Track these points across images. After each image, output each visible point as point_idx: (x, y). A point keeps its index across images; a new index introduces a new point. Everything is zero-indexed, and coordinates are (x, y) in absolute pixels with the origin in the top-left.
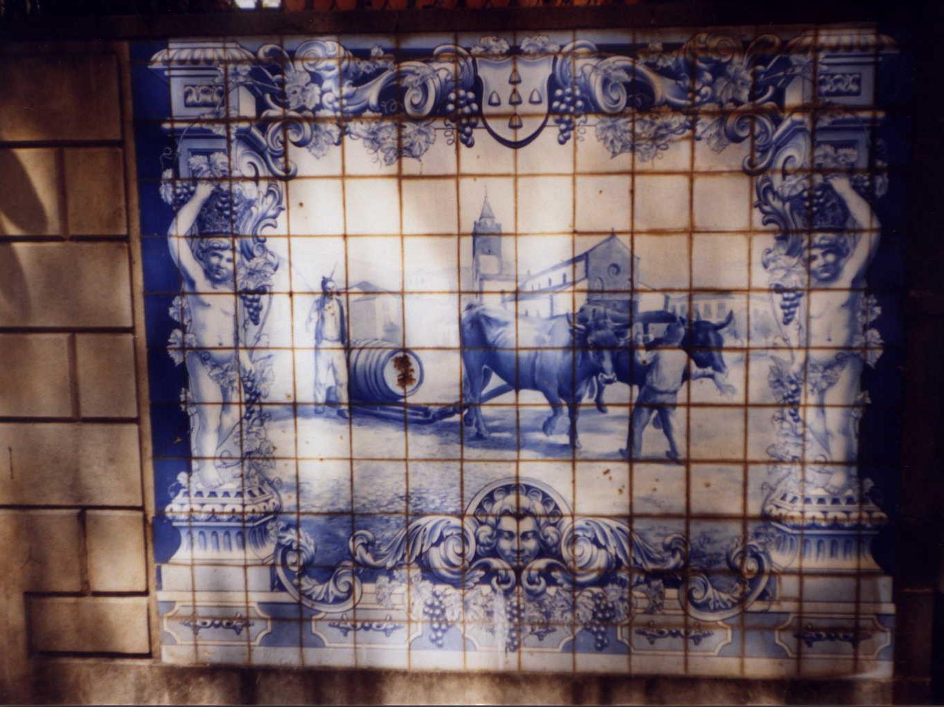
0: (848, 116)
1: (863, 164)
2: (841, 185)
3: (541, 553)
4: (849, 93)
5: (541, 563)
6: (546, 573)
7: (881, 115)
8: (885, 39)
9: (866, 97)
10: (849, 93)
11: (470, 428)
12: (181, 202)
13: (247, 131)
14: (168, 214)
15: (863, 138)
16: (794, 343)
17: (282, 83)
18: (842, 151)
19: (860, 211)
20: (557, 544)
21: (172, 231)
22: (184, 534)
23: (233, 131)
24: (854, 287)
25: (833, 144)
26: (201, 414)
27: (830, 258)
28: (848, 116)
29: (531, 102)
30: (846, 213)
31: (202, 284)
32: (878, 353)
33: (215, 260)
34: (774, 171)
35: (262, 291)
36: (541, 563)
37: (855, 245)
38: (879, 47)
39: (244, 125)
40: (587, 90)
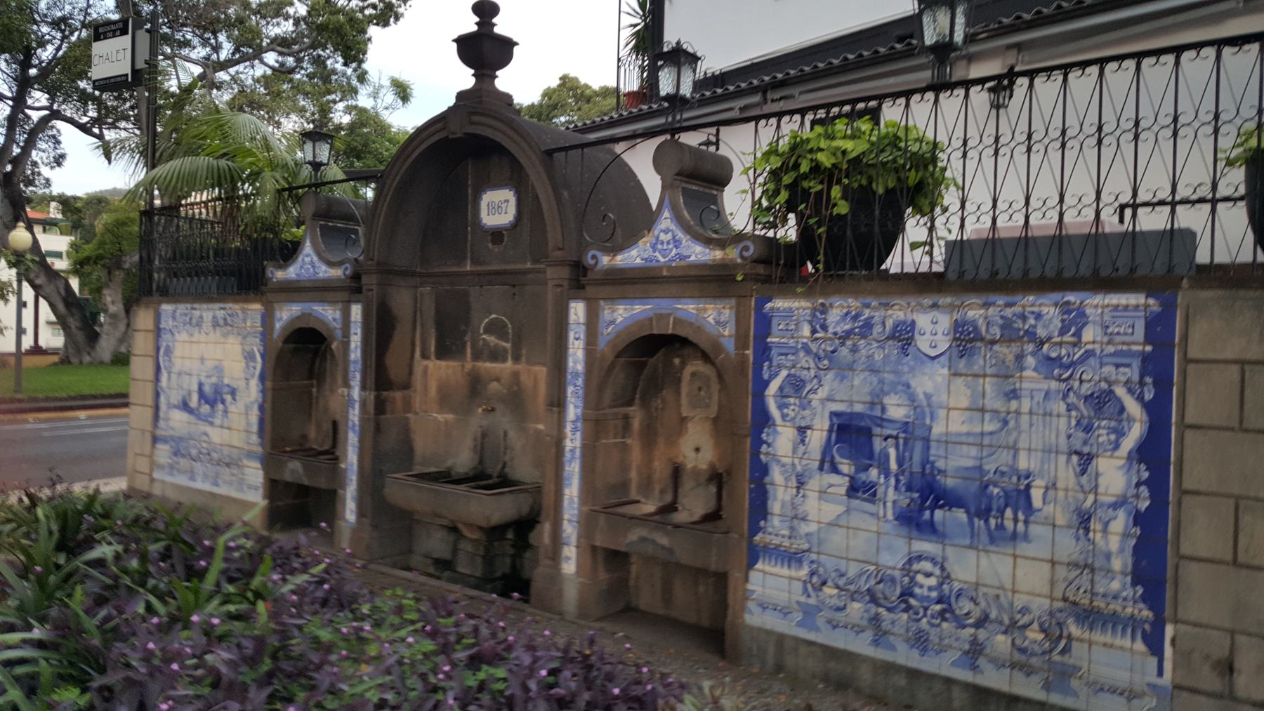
0: (1125, 348)
1: (1136, 378)
2: (1120, 391)
3: (939, 602)
4: (1126, 334)
5: (938, 607)
6: (942, 614)
7: (1149, 348)
8: (1151, 301)
9: (259, 325)
10: (1126, 334)
11: (469, 262)
12: (772, 377)
13: (806, 344)
14: (766, 384)
15: (1136, 364)
16: (1087, 488)
17: (825, 320)
18: (1122, 369)
19: (1133, 408)
20: (949, 597)
21: (767, 393)
22: (761, 554)
23: (328, 314)
24: (1129, 457)
25: (1117, 366)
26: (775, 490)
27: (1113, 437)
28: (1125, 348)
29: (931, 334)
30: (1122, 409)
31: (778, 420)
32: (1147, 503)
33: (785, 411)
34: (1075, 380)
35: (808, 427)
36: (938, 607)
37: (1130, 429)
38: (1147, 306)
39: (805, 340)
40: (976, 329)
